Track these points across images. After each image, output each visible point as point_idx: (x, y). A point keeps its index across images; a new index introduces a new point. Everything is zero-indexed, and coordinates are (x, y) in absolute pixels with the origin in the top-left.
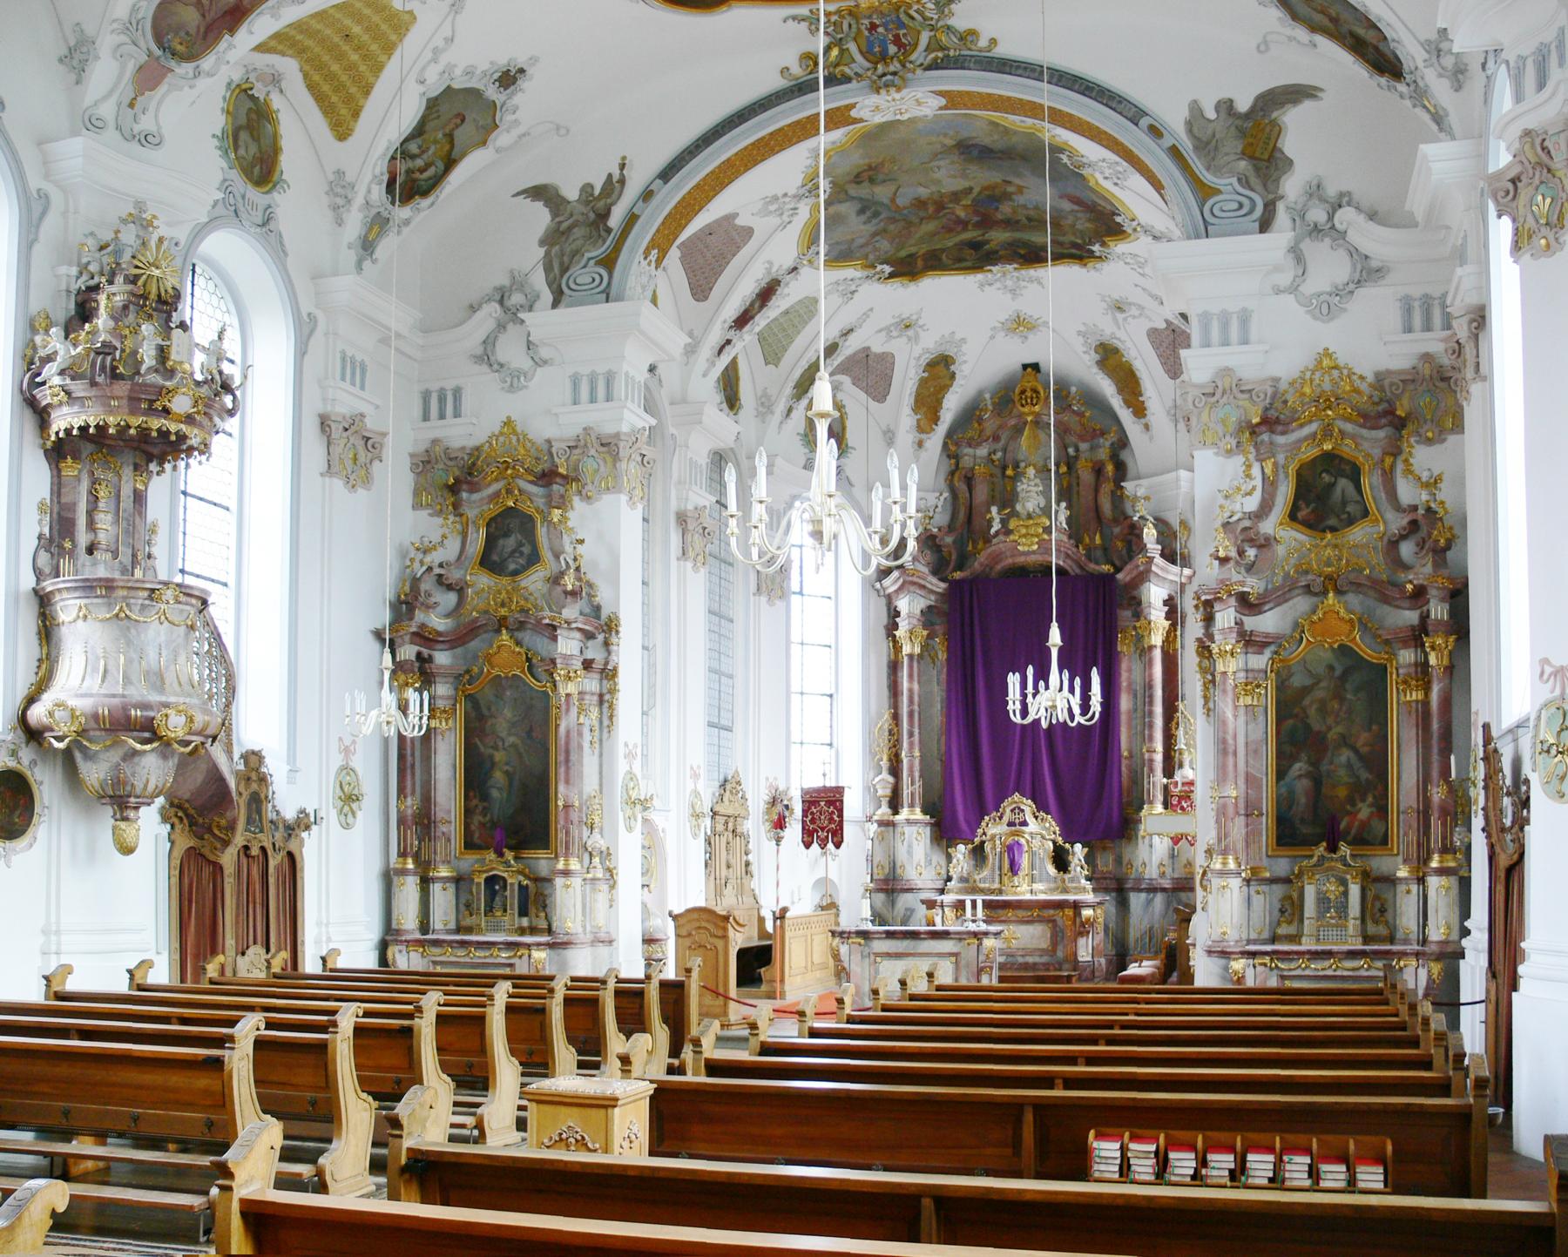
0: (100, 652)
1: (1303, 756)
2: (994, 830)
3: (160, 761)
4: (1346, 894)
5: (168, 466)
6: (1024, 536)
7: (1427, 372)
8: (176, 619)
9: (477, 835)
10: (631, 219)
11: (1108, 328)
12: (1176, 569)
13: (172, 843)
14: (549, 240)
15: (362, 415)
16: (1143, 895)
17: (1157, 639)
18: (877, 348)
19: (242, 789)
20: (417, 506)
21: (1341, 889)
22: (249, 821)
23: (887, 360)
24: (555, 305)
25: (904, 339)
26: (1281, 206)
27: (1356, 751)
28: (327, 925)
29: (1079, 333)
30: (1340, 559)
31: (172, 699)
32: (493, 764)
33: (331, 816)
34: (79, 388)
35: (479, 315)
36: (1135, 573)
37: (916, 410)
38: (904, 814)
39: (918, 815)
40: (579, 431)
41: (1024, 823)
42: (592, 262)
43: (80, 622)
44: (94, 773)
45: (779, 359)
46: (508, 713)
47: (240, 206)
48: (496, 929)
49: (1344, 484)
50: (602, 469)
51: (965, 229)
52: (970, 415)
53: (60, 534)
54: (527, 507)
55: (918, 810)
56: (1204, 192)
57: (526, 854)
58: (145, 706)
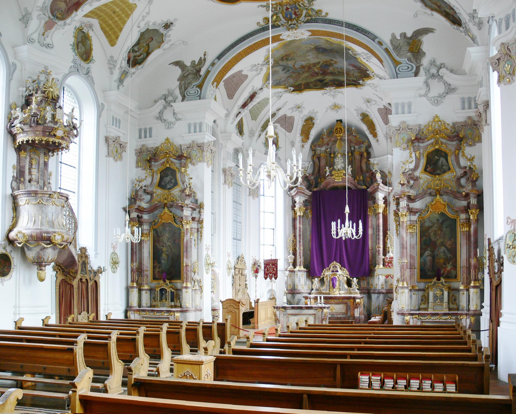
0: (33, 215)
1: (429, 249)
2: (327, 273)
3: (53, 251)
4: (443, 294)
5: (55, 154)
6: (337, 176)
7: (470, 123)
8: (58, 204)
9: (157, 275)
10: (208, 72)
11: (365, 108)
12: (387, 187)
13: (57, 277)
14: (181, 79)
15: (119, 137)
16: (376, 295)
17: (381, 210)
18: (289, 115)
19: (80, 260)
20: (137, 166)
21: (441, 293)
22: (82, 270)
23: (292, 119)
24: (183, 100)
25: (298, 112)
26: (421, 68)
27: (446, 247)
28: (108, 305)
29: (355, 110)
30: (441, 184)
31: (57, 230)
32: (162, 252)
33: (109, 269)
34: (26, 128)
35: (158, 104)
36: (373, 189)
37: (301, 135)
38: (298, 268)
39: (302, 268)
40: (191, 142)
41: (337, 271)
42: (195, 86)
43: (26, 205)
44: (31, 254)
45: (256, 118)
46: (167, 235)
47: (79, 68)
48: (163, 306)
49: (442, 159)
50: (198, 154)
51: (318, 75)
52: (319, 137)
53: (20, 176)
54: (173, 167)
55: (302, 267)
56: (396, 63)
57: (173, 281)
58: (48, 233)
